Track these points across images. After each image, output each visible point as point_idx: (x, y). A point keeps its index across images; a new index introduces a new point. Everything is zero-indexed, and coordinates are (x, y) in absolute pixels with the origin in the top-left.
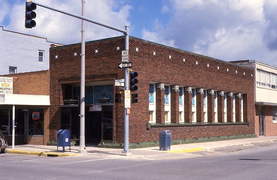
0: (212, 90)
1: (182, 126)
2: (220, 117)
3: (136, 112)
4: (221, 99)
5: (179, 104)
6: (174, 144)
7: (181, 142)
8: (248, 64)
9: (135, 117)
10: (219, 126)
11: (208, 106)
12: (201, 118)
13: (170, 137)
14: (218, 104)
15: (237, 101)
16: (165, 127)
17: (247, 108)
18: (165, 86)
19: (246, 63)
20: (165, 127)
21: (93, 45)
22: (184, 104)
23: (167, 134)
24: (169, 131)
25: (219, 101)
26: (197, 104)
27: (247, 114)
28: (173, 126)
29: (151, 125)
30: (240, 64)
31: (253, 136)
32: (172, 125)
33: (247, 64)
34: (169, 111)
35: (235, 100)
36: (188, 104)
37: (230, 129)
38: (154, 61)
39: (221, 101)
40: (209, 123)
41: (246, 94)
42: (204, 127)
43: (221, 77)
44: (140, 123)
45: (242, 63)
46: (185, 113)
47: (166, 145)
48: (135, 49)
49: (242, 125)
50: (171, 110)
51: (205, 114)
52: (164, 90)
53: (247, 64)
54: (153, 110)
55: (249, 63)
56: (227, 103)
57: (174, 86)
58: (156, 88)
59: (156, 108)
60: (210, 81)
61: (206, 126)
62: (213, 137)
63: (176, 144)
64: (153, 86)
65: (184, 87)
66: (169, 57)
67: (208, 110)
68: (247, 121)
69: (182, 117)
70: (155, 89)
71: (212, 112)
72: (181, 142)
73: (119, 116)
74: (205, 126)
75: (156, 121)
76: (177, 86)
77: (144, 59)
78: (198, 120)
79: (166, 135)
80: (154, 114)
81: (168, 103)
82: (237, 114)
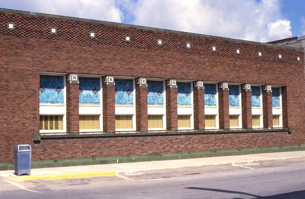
0: (107, 77)
1: (123, 136)
2: (222, 122)
3: (7, 118)
4: (223, 94)
5: (114, 104)
6: (100, 164)
7: (118, 160)
8: (297, 43)
9: (5, 125)
10: (215, 135)
11: (194, 106)
12: (171, 123)
13: (29, 154)
14: (219, 102)
15: (264, 98)
16: (79, 138)
17: (287, 106)
18: (229, 86)
19: (294, 41)
20: (79, 138)
21: (175, 52)
22: (136, 103)
23: (19, 151)
24: (28, 145)
25: (220, 98)
26: (166, 103)
27: (287, 116)
28: (265, 132)
29: (42, 136)
30: (287, 44)
31: (300, 148)
32: (243, 131)
33: (294, 43)
34: (280, 115)
35: (263, 95)
36: (139, 104)
37: (244, 138)
38: (53, 42)
39: (223, 97)
40: (244, 129)
41: (286, 86)
42: (178, 137)
43: (220, 62)
44: (18, 133)
45: (289, 43)
46: (194, 116)
47: (30, 167)
48: (258, 53)
49: (274, 133)
50: (103, 113)
51: (239, 117)
52: (77, 84)
53: (294, 43)
54: (100, 114)
55: (297, 41)
56: (242, 101)
57: (265, 87)
58: (218, 88)
59: (67, 111)
60: (193, 69)
61: (182, 136)
62: (200, 151)
63: (106, 163)
64: (63, 78)
65: (218, 83)
66: (297, 58)
67: (194, 112)
68: (287, 127)
69: (216, 121)
70: (240, 90)
71: (198, 114)
72: (118, 160)
73: (16, 121)
74: (180, 134)
75: (194, 128)
76: (248, 85)
77: (27, 40)
78: (168, 127)
79: (18, 152)
80: (281, 118)
81: (99, 103)
82: (265, 116)
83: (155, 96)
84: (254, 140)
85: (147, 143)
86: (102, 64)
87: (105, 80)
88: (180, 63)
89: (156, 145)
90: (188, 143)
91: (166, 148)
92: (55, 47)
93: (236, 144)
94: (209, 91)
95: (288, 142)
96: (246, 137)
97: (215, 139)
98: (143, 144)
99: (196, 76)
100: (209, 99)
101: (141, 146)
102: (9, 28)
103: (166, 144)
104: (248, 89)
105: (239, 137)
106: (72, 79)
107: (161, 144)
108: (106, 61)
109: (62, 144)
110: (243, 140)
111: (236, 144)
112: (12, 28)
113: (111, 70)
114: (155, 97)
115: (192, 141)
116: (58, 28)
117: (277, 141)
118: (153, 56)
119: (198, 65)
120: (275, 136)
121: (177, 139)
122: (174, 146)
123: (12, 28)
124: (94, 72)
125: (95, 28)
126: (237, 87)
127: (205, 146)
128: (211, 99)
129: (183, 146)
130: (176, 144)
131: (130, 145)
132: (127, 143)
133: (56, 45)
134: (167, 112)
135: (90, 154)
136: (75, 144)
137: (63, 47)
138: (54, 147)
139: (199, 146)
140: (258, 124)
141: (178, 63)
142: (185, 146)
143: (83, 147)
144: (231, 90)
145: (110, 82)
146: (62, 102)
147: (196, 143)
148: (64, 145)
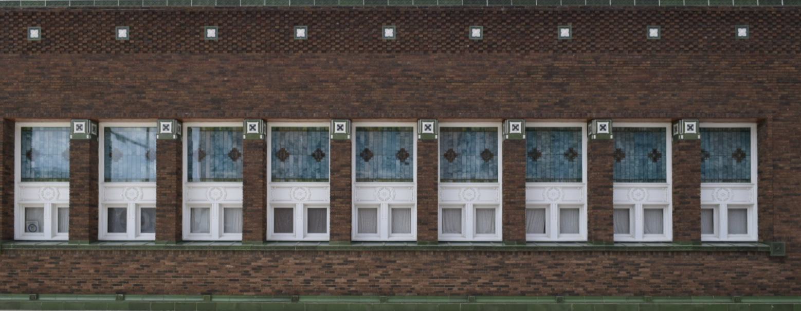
38: (32, 58)
52: (86, 141)
83: (557, 162)
84: (619, 275)
85: (257, 269)
86: (144, 95)
87: (676, 130)
88: (360, 78)
89: (285, 274)
90: (381, 275)
91: (312, 283)
92: (38, 68)
93: (549, 283)
94: (725, 146)
95: (769, 286)
96: (588, 264)
97: (471, 267)
98: (248, 271)
99: (412, 107)
100: (726, 167)
101: (242, 275)
102: (649, 37)
103: (314, 275)
104: (597, 134)
105: (562, 264)
106: (684, 131)
107: (300, 273)
108: (155, 88)
109: (51, 263)
110: (574, 272)
111: (549, 283)
112: (125, 36)
113: (167, 106)
114: (557, 166)
115: (392, 269)
116: (752, 27)
117: (716, 281)
118: (281, 68)
119: (419, 78)
120: (707, 268)
121: (346, 262)
122: (337, 280)
123: (125, 36)
124: (159, 113)
125: (500, 23)
126: (409, 131)
127: (435, 285)
128: (731, 166)
129: (365, 280)
130: (340, 276)
131: (214, 272)
132: (205, 266)
133: (39, 63)
134: (12, 188)
135: (111, 288)
136: (79, 263)
137: (56, 65)
138: (31, 268)
139: (416, 282)
140: (493, 231)
141: (353, 78)
142: (370, 281)
143: (97, 271)
144: (619, 138)
145: (424, 134)
146: (579, 180)
147: (408, 275)
148: (53, 266)
